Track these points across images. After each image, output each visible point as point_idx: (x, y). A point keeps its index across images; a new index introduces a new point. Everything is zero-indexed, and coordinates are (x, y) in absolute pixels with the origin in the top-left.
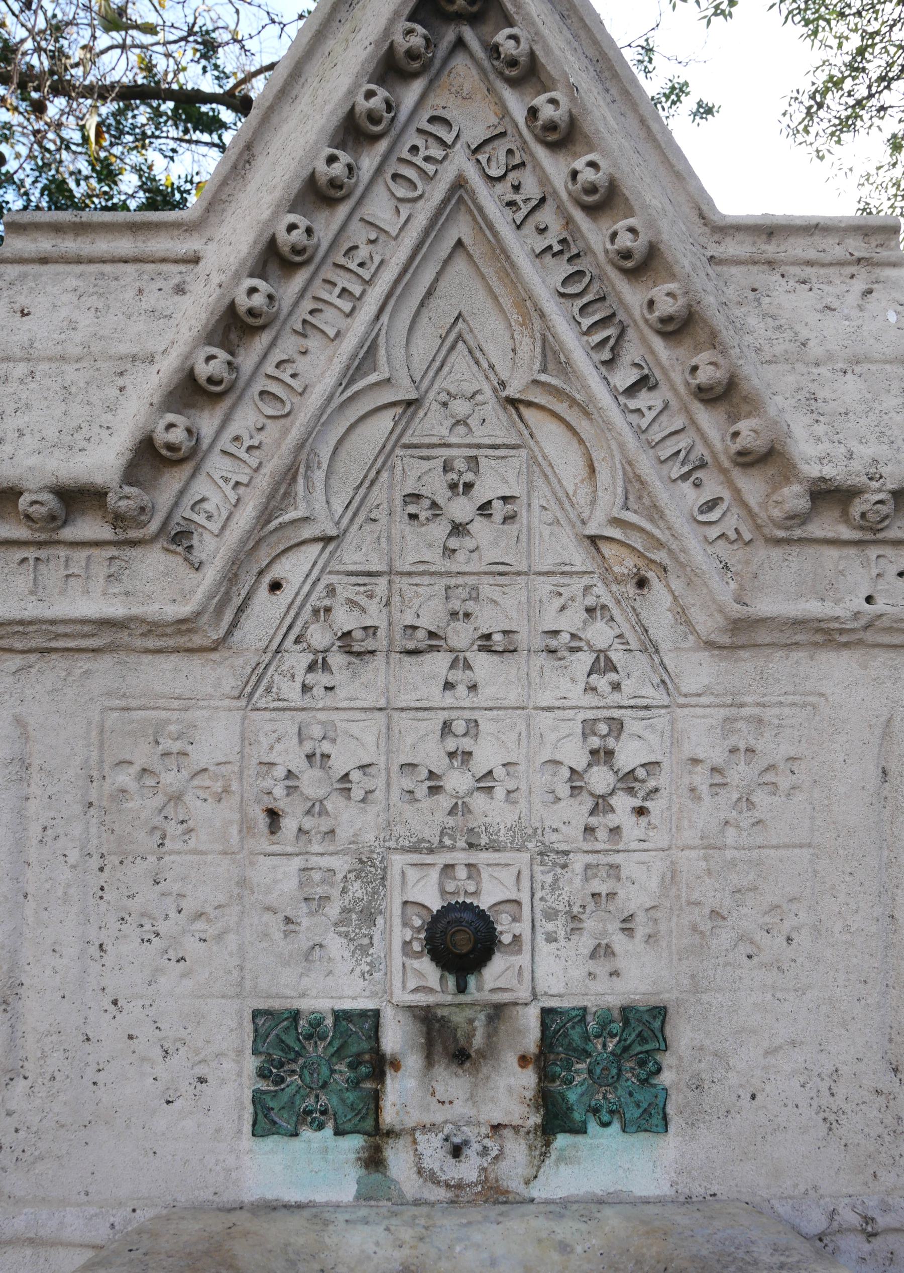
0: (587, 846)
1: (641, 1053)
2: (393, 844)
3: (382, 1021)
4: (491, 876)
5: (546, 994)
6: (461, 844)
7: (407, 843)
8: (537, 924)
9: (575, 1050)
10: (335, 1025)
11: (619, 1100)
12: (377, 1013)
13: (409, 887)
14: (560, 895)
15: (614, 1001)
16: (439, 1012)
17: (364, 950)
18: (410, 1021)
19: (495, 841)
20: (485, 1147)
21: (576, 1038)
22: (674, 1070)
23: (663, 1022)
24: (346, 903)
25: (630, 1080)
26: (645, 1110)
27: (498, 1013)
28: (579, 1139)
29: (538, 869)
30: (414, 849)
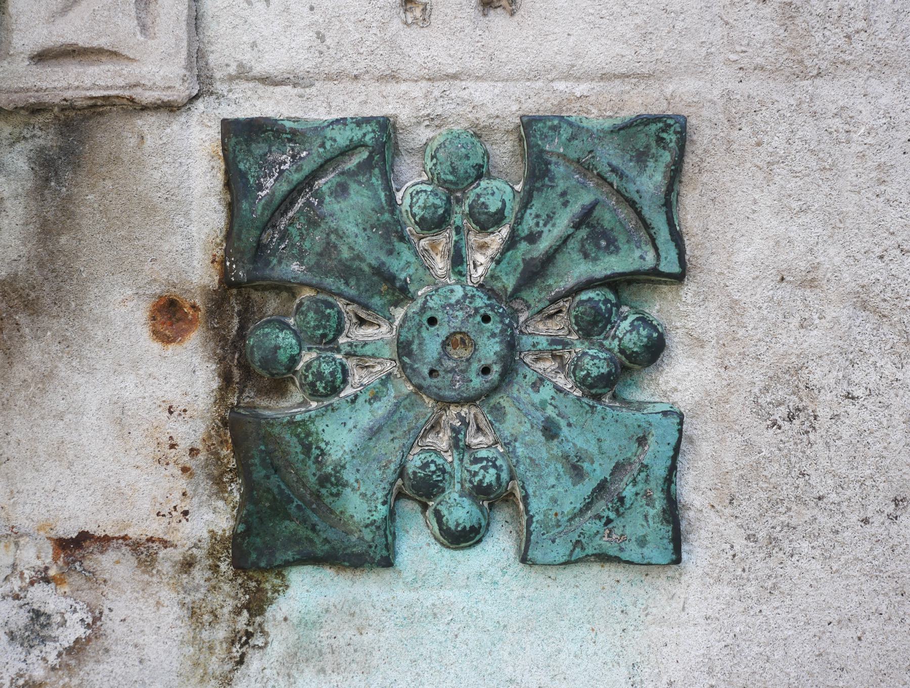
1: (590, 284)
5: (243, 74)
9: (346, 272)
11: (510, 453)
15: (499, 102)
20: (37, 614)
21: (350, 228)
22: (711, 353)
23: (675, 174)
25: (544, 386)
26: (602, 487)
28: (367, 588)
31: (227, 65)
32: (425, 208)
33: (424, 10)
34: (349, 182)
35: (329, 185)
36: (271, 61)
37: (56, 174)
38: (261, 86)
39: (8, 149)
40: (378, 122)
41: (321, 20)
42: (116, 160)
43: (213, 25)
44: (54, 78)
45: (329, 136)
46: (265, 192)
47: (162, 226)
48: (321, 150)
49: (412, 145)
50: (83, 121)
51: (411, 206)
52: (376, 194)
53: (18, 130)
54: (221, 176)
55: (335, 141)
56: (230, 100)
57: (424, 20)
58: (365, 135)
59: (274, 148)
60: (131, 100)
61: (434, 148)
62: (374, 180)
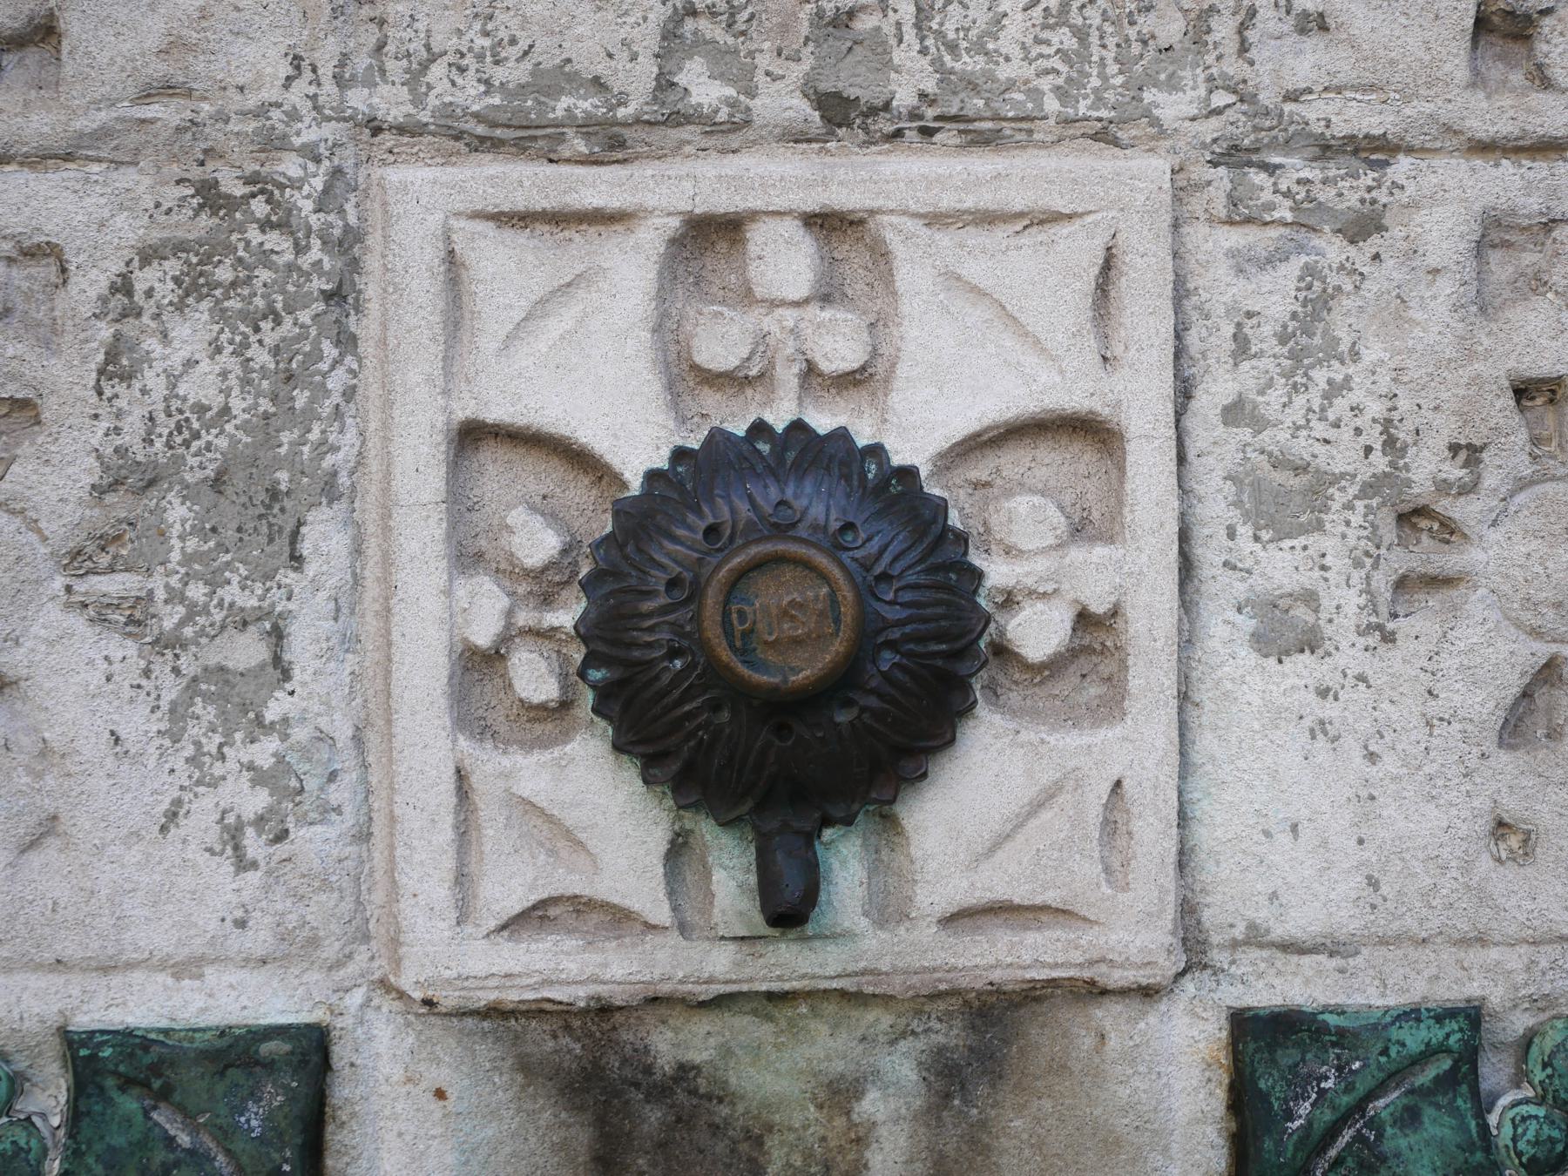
0: (1491, 116)
2: (391, 102)
3: (342, 1091)
4: (953, 279)
5: (1255, 938)
6: (782, 101)
7: (470, 95)
8: (1209, 556)
10: (75, 1116)
12: (312, 1050)
13: (488, 344)
14: (1335, 389)
16: (669, 1044)
17: (238, 701)
18: (502, 1088)
19: (972, 86)
24: (133, 426)
27: (989, 1037)
29: (1214, 244)
30: (514, 133)
31: (1232, 926)
32: (1537, 1143)
33: (1525, 841)
34: (1420, 1104)
35: (1392, 1108)
36: (1299, 922)
37: (963, 1087)
38: (1279, 955)
39: (887, 1049)
40: (1468, 1017)
41: (1374, 859)
42: (1063, 1069)
43: (1210, 866)
44: (975, 952)
45: (1394, 1037)
46: (1297, 1123)
47: (1129, 1168)
48: (1383, 1059)
49: (1501, 1037)
50: (1007, 1009)
51: (1514, 1139)
52: (1463, 1122)
53: (903, 1021)
54: (1221, 1094)
55: (1404, 1045)
56: (1232, 976)
57: (1526, 854)
58: (1448, 1036)
59: (1309, 1056)
60: (1092, 983)
61: (1547, 1052)
62: (1460, 1102)
